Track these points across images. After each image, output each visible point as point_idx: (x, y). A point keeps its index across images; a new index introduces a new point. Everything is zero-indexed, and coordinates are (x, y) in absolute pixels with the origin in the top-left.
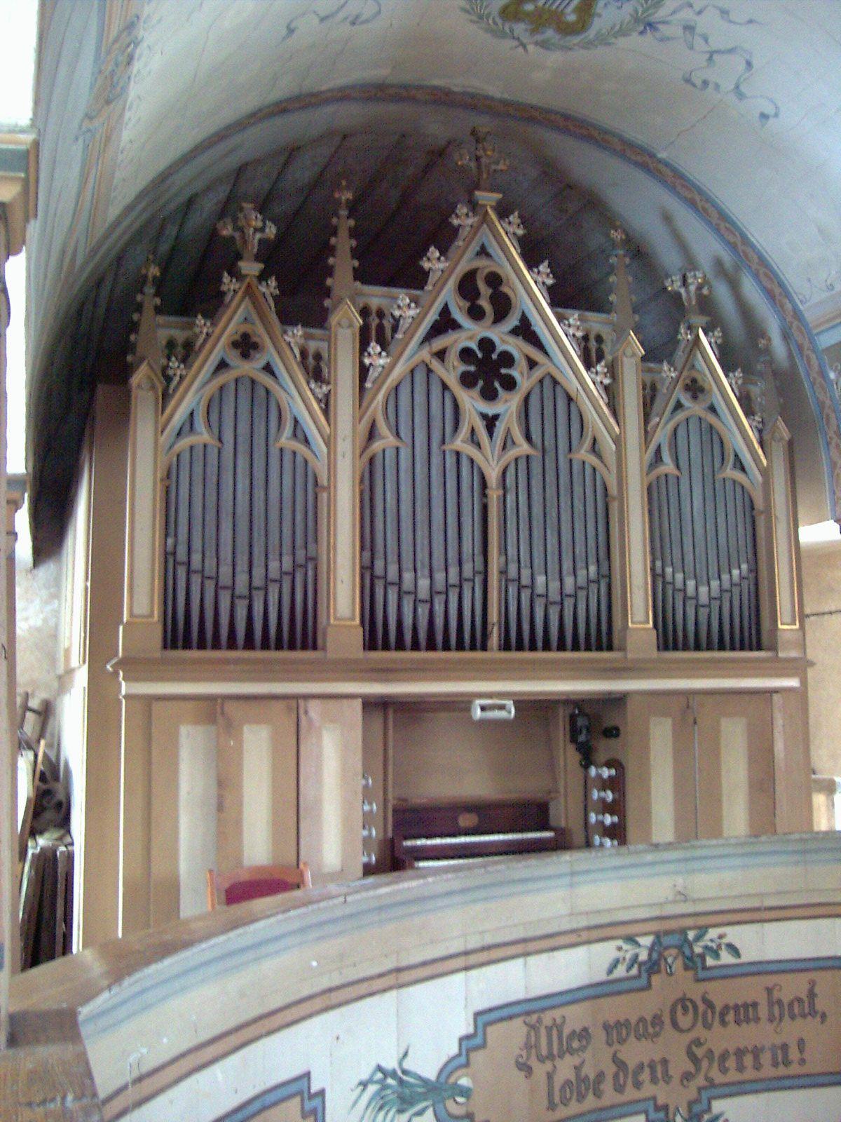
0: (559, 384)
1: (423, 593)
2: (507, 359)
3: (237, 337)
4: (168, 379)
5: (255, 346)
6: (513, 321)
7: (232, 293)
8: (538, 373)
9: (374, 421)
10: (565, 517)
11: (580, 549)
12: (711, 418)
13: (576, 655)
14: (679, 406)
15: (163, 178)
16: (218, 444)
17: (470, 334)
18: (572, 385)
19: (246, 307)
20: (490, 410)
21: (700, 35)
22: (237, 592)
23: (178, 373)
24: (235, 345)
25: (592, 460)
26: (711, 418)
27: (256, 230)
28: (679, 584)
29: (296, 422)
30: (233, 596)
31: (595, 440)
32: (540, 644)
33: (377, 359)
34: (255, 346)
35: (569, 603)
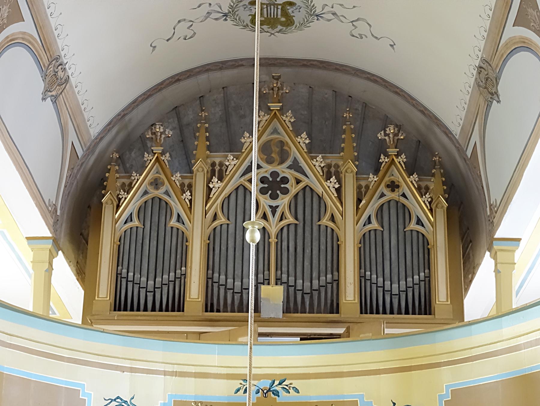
0: (247, 189)
1: (150, 288)
2: (285, 180)
3: (152, 181)
4: (120, 200)
5: (398, 187)
6: (289, 162)
7: (149, 161)
8: (301, 185)
9: (283, 212)
10: (315, 252)
11: (323, 267)
12: (402, 200)
13: (377, 316)
14: (382, 195)
15: (122, 116)
16: (143, 227)
17: (265, 170)
18: (319, 190)
19: (157, 168)
20: (274, 203)
21: (340, 16)
22: (386, 289)
23: (124, 197)
24: (388, 186)
25: (331, 224)
26: (402, 200)
27: (161, 133)
28: (380, 284)
29: (179, 215)
30: (146, 292)
31: (178, 214)
32: (403, 311)
33: (215, 183)
34: (398, 187)
35: (158, 292)
